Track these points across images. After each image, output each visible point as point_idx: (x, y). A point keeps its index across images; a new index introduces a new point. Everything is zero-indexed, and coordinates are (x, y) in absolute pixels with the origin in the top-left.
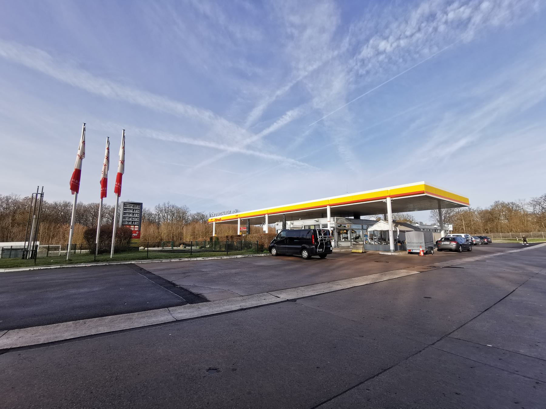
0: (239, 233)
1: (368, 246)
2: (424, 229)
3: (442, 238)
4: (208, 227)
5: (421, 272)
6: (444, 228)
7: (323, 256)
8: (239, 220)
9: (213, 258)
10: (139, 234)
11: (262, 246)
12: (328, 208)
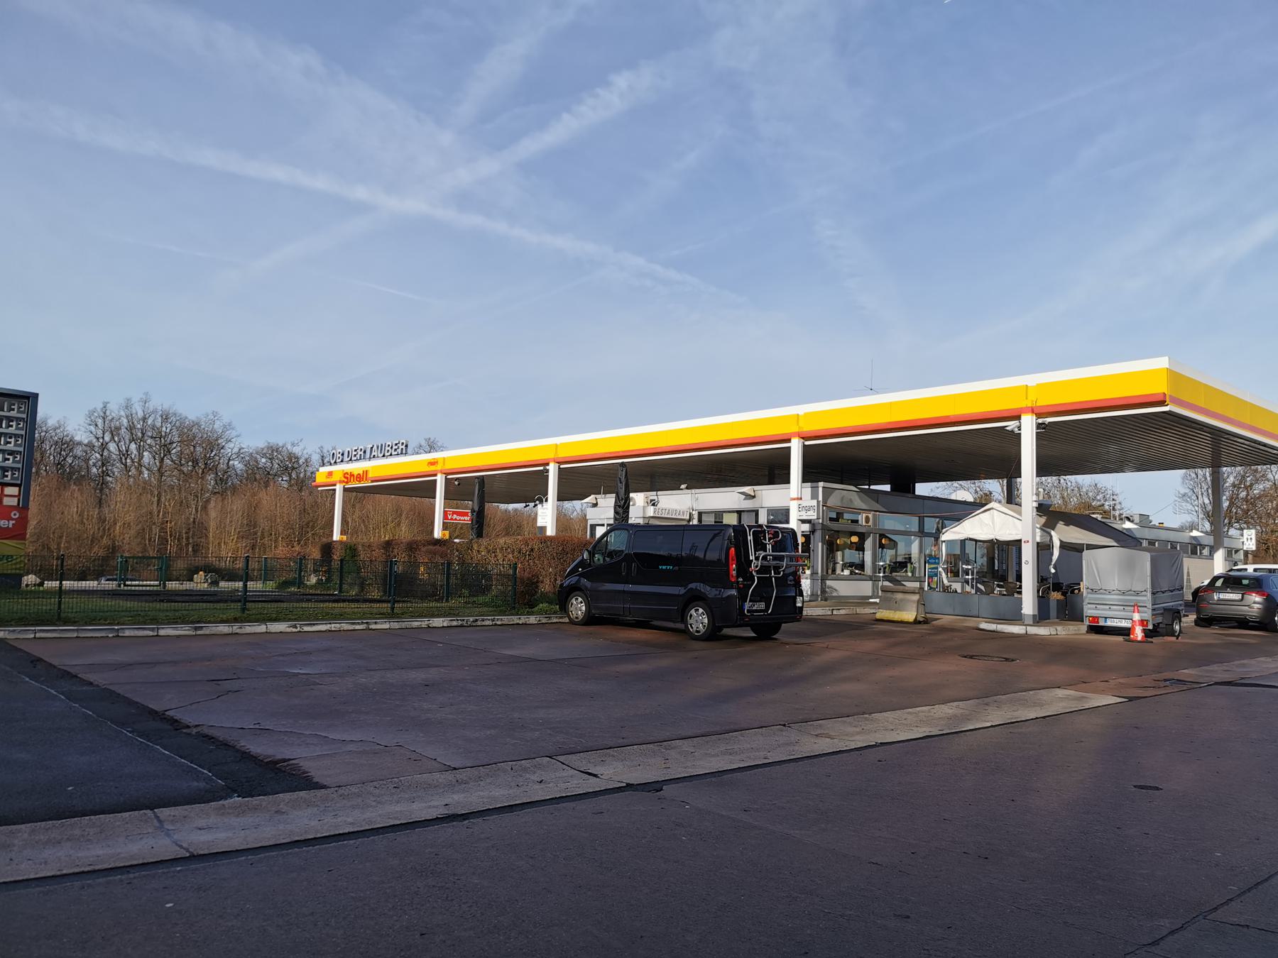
0: (438, 533)
1: (937, 597)
2: (1152, 543)
3: (1216, 579)
4: (311, 501)
5: (1131, 699)
6: (1227, 542)
7: (766, 630)
8: (440, 480)
9: (333, 627)
10: (23, 522)
11: (533, 583)
12: (796, 448)
